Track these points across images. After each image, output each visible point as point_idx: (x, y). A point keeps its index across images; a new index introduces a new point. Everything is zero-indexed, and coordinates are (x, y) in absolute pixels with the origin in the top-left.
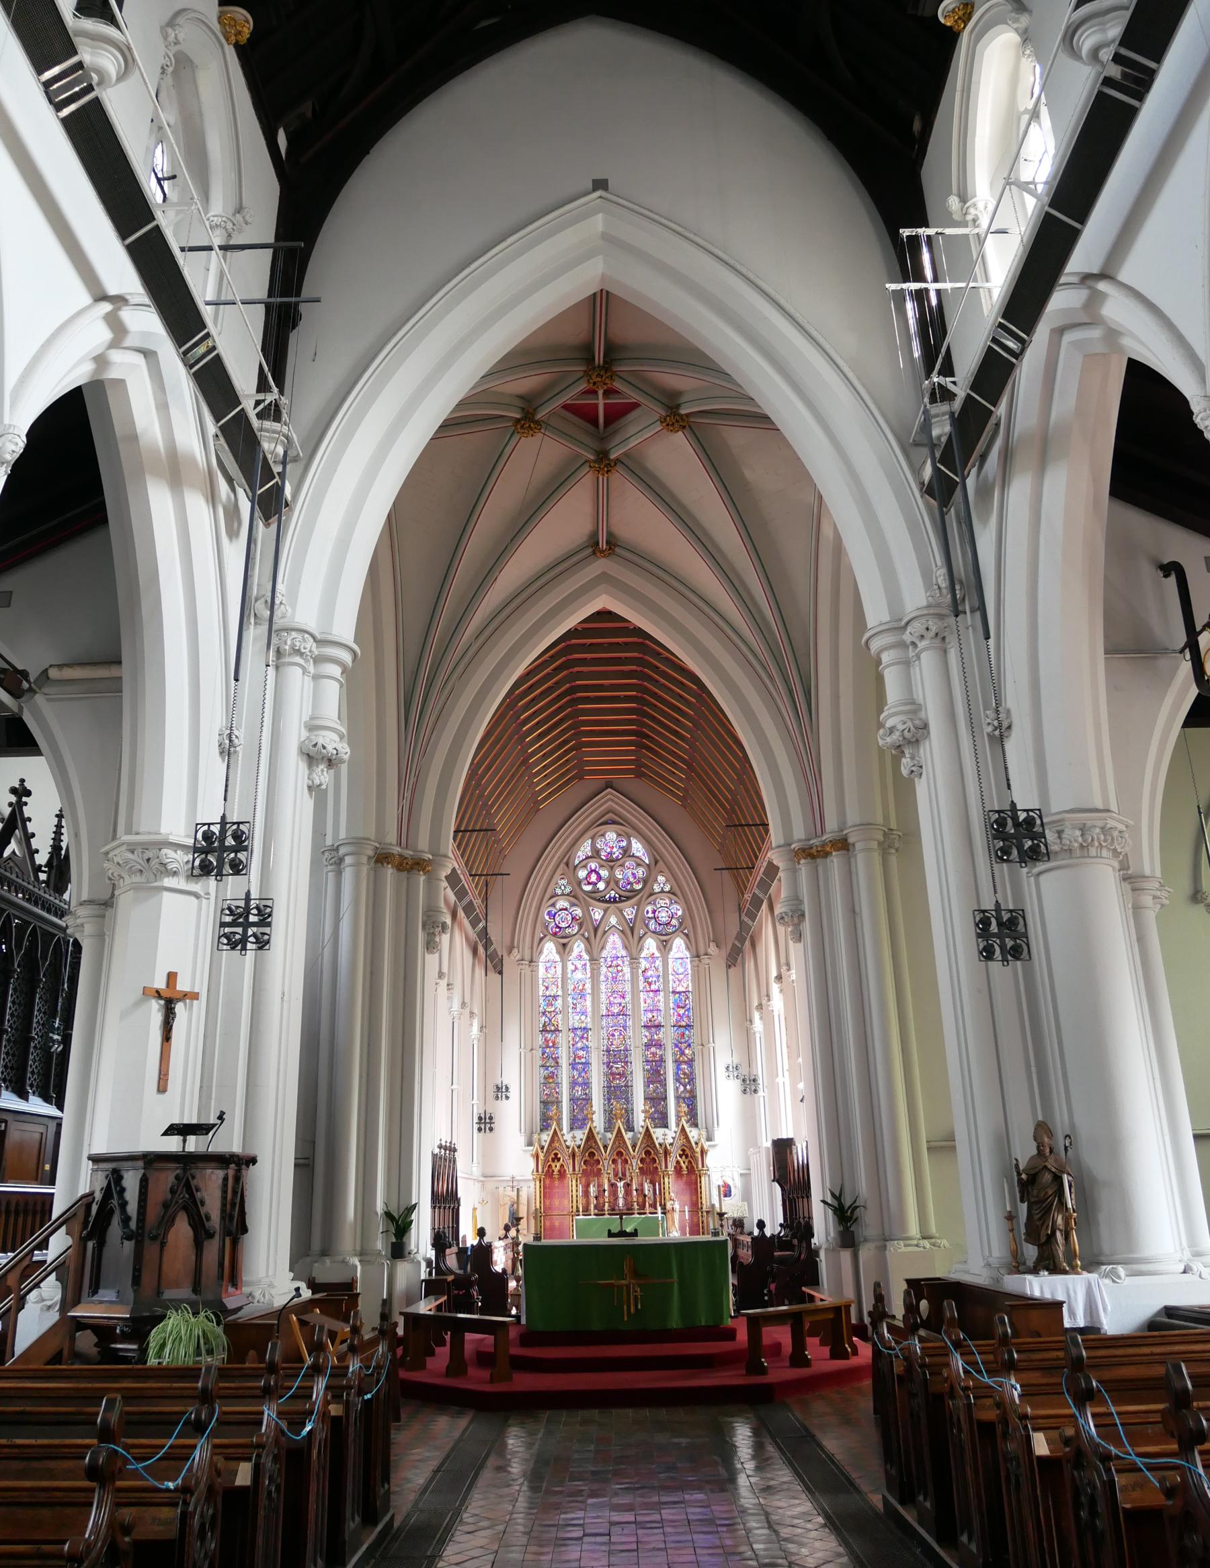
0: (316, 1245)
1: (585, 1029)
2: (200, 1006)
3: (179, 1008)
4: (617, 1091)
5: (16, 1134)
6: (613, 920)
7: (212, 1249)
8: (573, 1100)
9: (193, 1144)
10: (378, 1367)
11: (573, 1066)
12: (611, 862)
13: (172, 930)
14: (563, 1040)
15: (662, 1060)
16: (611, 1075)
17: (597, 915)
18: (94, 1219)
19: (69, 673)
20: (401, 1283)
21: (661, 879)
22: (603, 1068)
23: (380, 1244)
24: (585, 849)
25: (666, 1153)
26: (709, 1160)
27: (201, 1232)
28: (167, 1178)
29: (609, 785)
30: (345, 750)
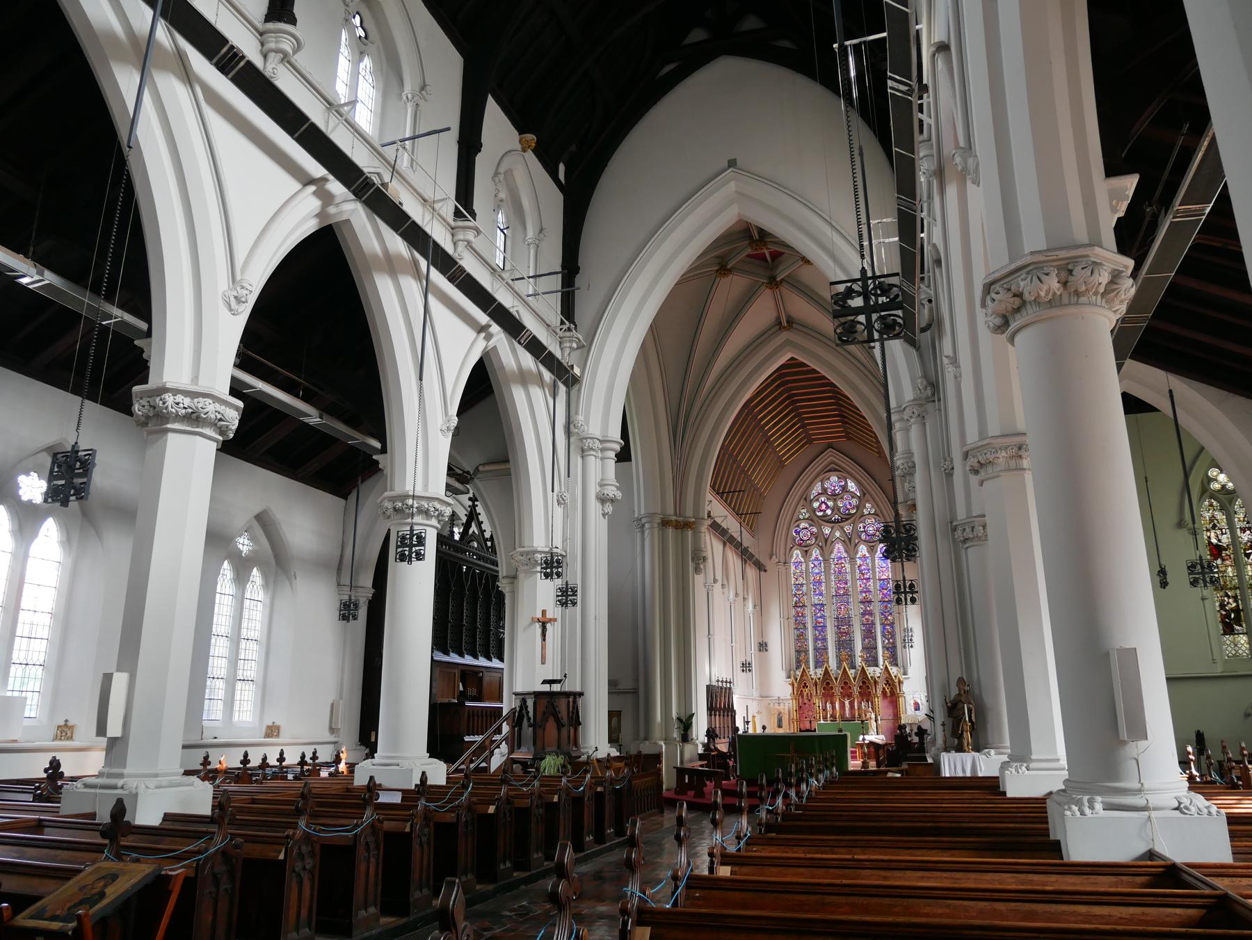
0: (642, 735)
1: (822, 605)
2: (558, 624)
3: (548, 626)
4: (844, 644)
5: (487, 677)
6: (838, 534)
7: (564, 731)
8: (816, 649)
9: (556, 688)
10: (624, 778)
11: (815, 628)
12: (834, 497)
13: (539, 594)
14: (808, 612)
15: (873, 624)
16: (840, 633)
17: (827, 531)
18: (517, 718)
19: (487, 468)
20: (687, 756)
21: (868, 505)
22: (835, 629)
23: (676, 735)
24: (817, 488)
25: (876, 682)
26: (905, 688)
27: (560, 725)
28: (544, 701)
29: (830, 446)
30: (619, 495)
